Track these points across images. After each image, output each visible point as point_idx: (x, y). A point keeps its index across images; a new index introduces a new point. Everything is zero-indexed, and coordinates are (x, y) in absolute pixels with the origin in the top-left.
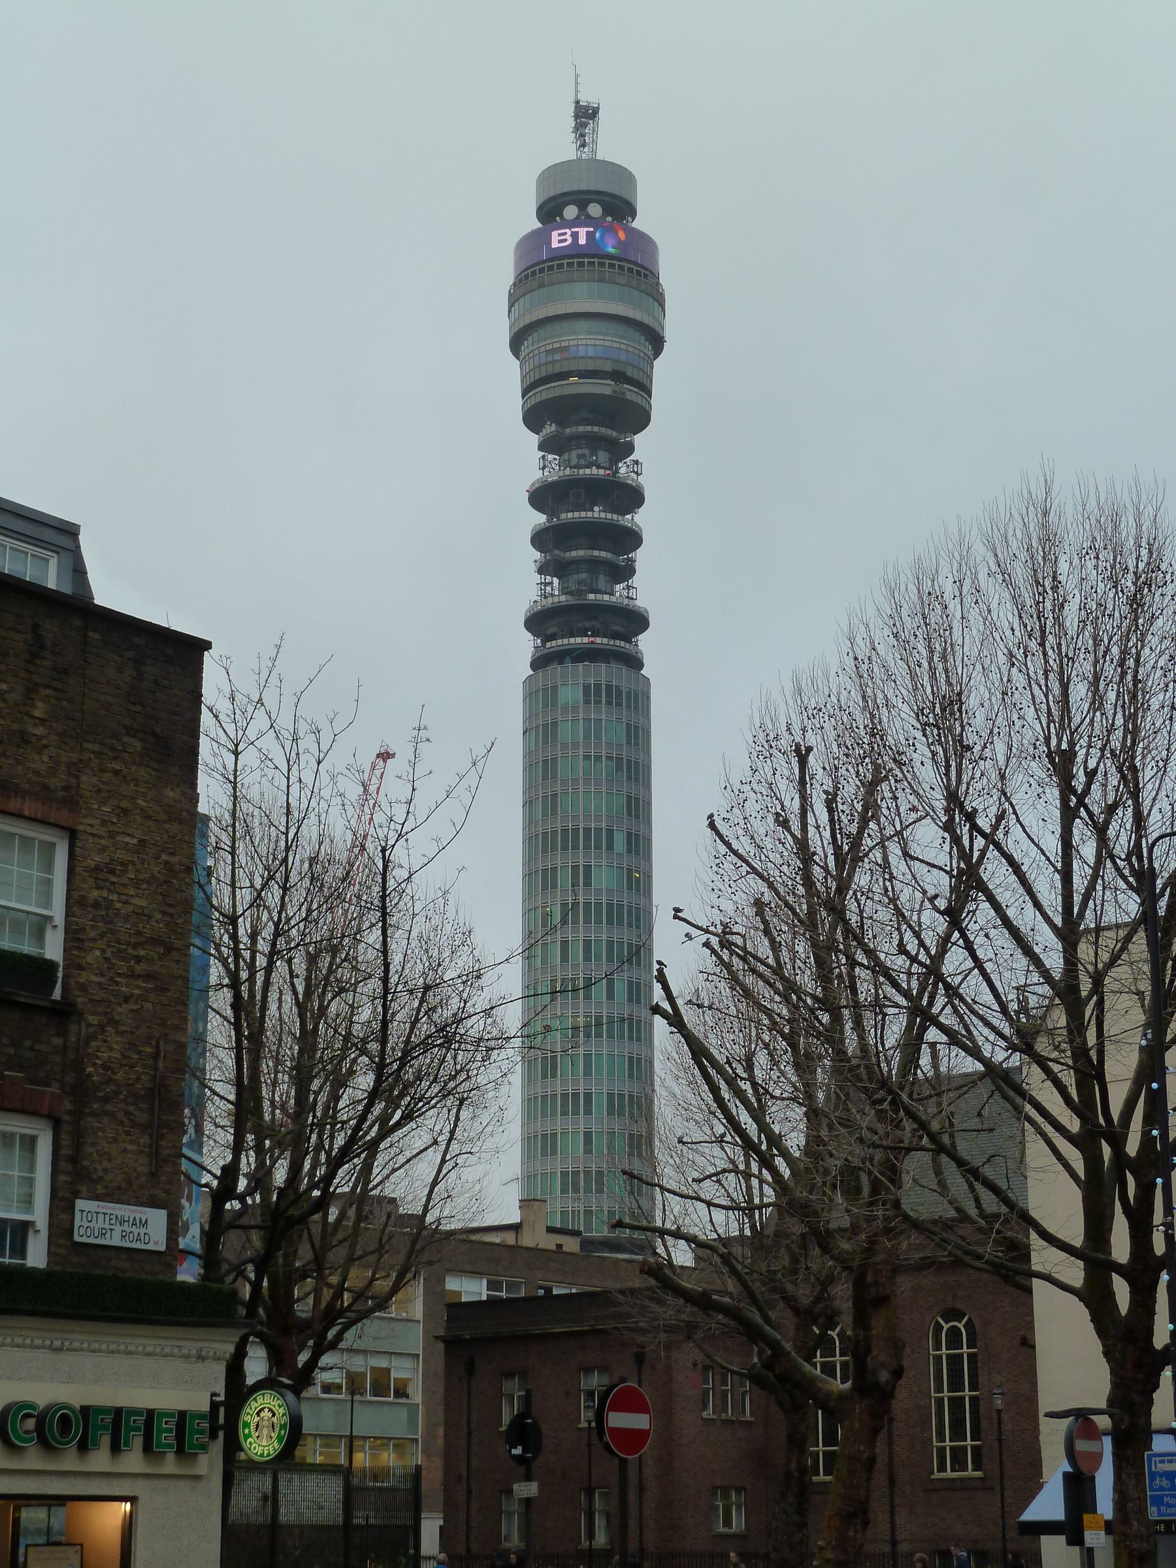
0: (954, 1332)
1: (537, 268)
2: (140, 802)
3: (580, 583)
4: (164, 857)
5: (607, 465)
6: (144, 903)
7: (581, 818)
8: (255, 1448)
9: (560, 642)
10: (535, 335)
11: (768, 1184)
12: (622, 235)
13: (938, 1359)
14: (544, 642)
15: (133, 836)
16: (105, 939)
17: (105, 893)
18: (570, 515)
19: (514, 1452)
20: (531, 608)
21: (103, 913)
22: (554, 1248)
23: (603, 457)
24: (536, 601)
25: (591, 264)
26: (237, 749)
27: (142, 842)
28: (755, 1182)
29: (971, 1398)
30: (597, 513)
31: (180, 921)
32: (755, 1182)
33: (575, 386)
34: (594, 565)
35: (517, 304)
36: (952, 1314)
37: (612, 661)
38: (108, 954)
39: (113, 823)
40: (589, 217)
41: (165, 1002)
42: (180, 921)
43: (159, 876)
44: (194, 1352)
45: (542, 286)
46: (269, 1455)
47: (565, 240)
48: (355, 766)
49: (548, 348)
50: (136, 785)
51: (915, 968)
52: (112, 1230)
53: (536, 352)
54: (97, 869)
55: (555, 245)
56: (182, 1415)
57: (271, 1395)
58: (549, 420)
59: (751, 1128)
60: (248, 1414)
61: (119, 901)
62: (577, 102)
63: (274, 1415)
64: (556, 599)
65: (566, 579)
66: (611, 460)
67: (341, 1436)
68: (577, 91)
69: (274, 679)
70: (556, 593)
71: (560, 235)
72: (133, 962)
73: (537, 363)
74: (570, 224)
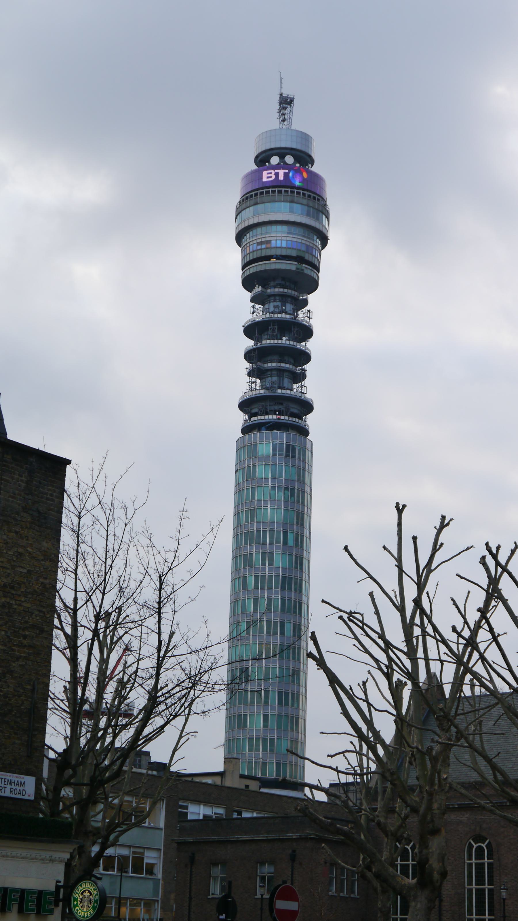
0: (480, 850)
1: (253, 193)
2: (29, 549)
3: (273, 383)
4: (41, 580)
5: (291, 312)
6: (28, 605)
7: (268, 524)
8: (80, 913)
9: (259, 418)
10: (251, 233)
11: (372, 760)
12: (305, 175)
13: (470, 865)
14: (250, 418)
15: (24, 568)
16: (7, 625)
17: (8, 600)
18: (268, 342)
19: (221, 917)
20: (243, 396)
21: (7, 611)
22: (243, 787)
23: (289, 307)
24: (246, 393)
25: (286, 192)
26: (80, 515)
27: (29, 572)
28: (365, 759)
29: (489, 890)
30: (284, 341)
31: (48, 616)
32: (365, 759)
33: (274, 264)
34: (281, 372)
35: (240, 214)
36: (479, 839)
37: (290, 430)
38: (9, 634)
39: (14, 561)
40: (285, 163)
41: (38, 661)
42: (48, 616)
43: (38, 591)
44: (48, 857)
45: (256, 204)
46: (87, 917)
47: (271, 177)
48: (145, 528)
49: (259, 241)
50: (27, 540)
51: (462, 641)
52: (5, 787)
53: (251, 243)
54: (5, 586)
55: (265, 179)
56: (40, 892)
57: (90, 883)
58: (258, 284)
59: (364, 728)
60: (77, 893)
61: (16, 604)
62: (281, 95)
63: (91, 894)
64: (258, 392)
65: (264, 380)
66: (294, 310)
67: (113, 897)
68: (281, 88)
69: (102, 476)
70: (258, 388)
71: (268, 174)
72: (22, 638)
73: (251, 250)
74: (274, 168)
